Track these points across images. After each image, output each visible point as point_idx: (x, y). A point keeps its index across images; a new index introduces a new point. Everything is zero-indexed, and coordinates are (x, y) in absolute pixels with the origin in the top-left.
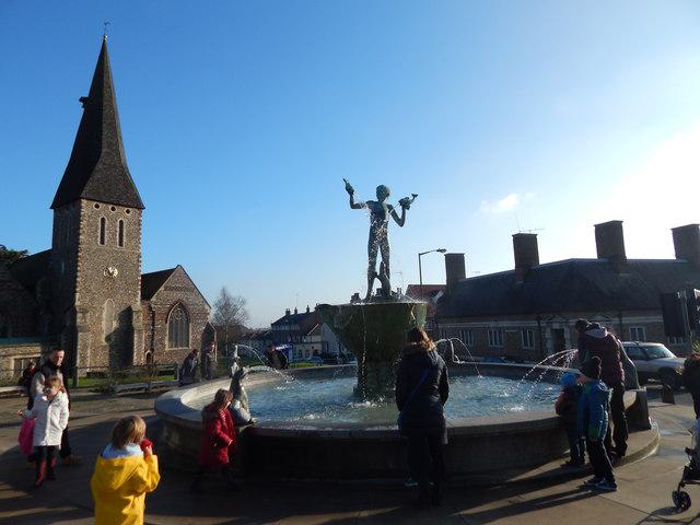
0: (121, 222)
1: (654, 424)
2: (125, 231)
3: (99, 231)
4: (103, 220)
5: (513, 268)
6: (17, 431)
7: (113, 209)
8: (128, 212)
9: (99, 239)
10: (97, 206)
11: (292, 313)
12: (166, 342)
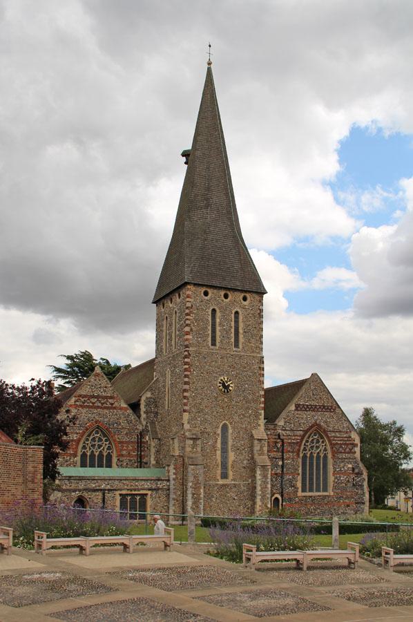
3: (210, 328)
7: (226, 296)
8: (245, 299)
12: (299, 484)
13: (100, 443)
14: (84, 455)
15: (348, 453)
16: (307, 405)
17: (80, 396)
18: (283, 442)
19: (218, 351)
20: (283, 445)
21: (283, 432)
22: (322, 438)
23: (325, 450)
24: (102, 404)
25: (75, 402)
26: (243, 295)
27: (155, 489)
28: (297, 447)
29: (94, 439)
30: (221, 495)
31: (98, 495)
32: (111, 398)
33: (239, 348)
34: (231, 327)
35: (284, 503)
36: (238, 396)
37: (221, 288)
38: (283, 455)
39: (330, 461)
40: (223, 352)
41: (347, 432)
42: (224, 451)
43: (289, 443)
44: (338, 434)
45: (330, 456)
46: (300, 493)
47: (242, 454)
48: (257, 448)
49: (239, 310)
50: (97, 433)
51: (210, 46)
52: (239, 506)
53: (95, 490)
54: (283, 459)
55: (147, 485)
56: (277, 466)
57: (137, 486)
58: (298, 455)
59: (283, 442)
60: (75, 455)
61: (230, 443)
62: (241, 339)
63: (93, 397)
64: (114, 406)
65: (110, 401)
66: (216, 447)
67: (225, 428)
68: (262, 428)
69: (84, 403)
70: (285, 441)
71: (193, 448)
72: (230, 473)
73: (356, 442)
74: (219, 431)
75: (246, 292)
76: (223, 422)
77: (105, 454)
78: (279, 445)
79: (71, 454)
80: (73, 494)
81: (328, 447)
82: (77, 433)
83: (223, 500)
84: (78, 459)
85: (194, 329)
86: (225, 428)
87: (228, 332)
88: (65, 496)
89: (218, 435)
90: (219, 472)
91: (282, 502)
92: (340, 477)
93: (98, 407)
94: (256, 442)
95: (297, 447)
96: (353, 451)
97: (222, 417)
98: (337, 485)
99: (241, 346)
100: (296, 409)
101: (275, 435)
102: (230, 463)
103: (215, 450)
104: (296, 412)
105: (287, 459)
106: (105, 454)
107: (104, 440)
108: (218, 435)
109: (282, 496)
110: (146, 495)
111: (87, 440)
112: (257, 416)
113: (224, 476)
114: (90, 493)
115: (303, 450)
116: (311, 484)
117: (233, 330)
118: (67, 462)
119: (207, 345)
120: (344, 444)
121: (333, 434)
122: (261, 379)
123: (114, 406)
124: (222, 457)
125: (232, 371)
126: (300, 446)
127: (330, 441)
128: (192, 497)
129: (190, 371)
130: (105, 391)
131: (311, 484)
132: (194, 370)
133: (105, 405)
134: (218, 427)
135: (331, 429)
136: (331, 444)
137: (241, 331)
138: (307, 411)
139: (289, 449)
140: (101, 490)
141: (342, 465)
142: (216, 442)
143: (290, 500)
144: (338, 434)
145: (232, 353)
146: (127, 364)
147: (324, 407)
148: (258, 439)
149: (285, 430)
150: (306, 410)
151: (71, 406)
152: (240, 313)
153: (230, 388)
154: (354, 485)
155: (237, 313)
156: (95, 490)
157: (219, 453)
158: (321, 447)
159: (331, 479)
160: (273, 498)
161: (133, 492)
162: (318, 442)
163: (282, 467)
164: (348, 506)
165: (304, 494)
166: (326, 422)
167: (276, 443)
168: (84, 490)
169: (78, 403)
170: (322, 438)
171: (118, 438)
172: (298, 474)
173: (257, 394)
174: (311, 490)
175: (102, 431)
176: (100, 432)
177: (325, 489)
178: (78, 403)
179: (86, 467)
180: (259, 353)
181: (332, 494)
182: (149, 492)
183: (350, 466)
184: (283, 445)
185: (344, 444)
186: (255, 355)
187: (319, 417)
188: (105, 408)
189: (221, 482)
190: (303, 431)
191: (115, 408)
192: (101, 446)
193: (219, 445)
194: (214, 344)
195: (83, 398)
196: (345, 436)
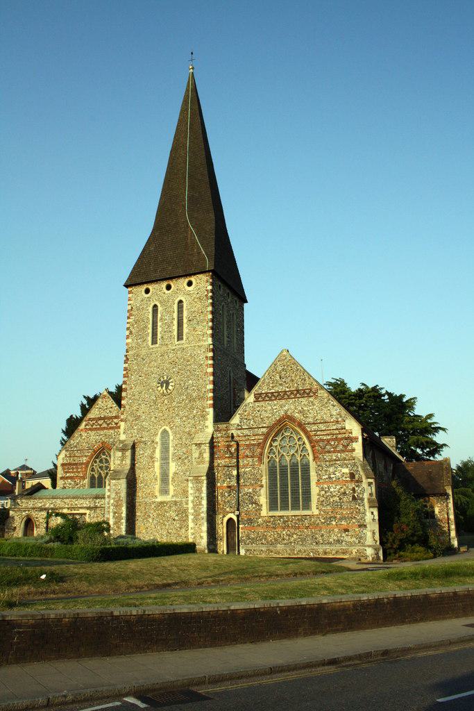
3: (150, 326)
8: (190, 284)
9: (150, 338)
12: (263, 500)
13: (101, 465)
14: (93, 478)
15: (342, 451)
16: (272, 393)
17: (90, 419)
18: (238, 445)
20: (237, 450)
21: (239, 432)
22: (297, 433)
23: (304, 449)
24: (108, 424)
25: (85, 426)
26: (187, 280)
27: (93, 508)
28: (259, 450)
30: (159, 515)
32: (116, 417)
34: (173, 319)
35: (241, 526)
36: (181, 394)
38: (238, 462)
40: (165, 348)
41: (337, 422)
42: (165, 459)
43: (247, 445)
44: (322, 427)
47: (185, 464)
51: (192, 53)
52: (181, 528)
54: (238, 467)
55: (86, 503)
56: (230, 476)
57: (76, 505)
58: (260, 460)
59: (238, 445)
60: (84, 478)
62: (185, 330)
63: (100, 419)
69: (92, 426)
70: (241, 443)
71: (122, 460)
72: (171, 488)
73: (354, 435)
74: (158, 439)
76: (163, 428)
78: (233, 450)
80: (24, 513)
81: (308, 446)
83: (161, 521)
84: (86, 481)
85: (133, 331)
87: (170, 325)
89: (157, 443)
90: (157, 487)
91: (238, 524)
93: (104, 428)
95: (259, 450)
96: (349, 448)
100: (257, 400)
101: (228, 437)
102: (171, 475)
104: (257, 404)
105: (245, 466)
108: (157, 443)
110: (85, 514)
112: (204, 417)
113: (164, 491)
116: (284, 493)
117: (175, 322)
118: (77, 485)
120: (333, 440)
121: (315, 427)
124: (162, 467)
126: (263, 448)
127: (309, 437)
128: (114, 517)
129: (128, 377)
131: (284, 493)
133: (110, 426)
135: (311, 420)
136: (310, 442)
139: (248, 453)
140: (45, 509)
141: (331, 469)
142: (154, 451)
143: (250, 521)
144: (322, 427)
146: (403, 394)
147: (298, 391)
150: (270, 400)
151: (82, 430)
152: (184, 300)
154: (354, 498)
155: (181, 302)
157: (157, 465)
159: (314, 490)
161: (73, 512)
163: (238, 476)
164: (346, 530)
165: (271, 513)
167: (229, 446)
168: (34, 508)
169: (87, 427)
170: (297, 433)
172: (262, 486)
173: (204, 390)
174: (285, 508)
177: (307, 506)
178: (87, 427)
179: (95, 487)
181: (316, 512)
182: (88, 512)
183: (346, 470)
184: (237, 450)
185: (333, 440)
186: (201, 343)
188: (111, 428)
189: (160, 499)
190: (267, 427)
193: (158, 454)
196: (334, 427)
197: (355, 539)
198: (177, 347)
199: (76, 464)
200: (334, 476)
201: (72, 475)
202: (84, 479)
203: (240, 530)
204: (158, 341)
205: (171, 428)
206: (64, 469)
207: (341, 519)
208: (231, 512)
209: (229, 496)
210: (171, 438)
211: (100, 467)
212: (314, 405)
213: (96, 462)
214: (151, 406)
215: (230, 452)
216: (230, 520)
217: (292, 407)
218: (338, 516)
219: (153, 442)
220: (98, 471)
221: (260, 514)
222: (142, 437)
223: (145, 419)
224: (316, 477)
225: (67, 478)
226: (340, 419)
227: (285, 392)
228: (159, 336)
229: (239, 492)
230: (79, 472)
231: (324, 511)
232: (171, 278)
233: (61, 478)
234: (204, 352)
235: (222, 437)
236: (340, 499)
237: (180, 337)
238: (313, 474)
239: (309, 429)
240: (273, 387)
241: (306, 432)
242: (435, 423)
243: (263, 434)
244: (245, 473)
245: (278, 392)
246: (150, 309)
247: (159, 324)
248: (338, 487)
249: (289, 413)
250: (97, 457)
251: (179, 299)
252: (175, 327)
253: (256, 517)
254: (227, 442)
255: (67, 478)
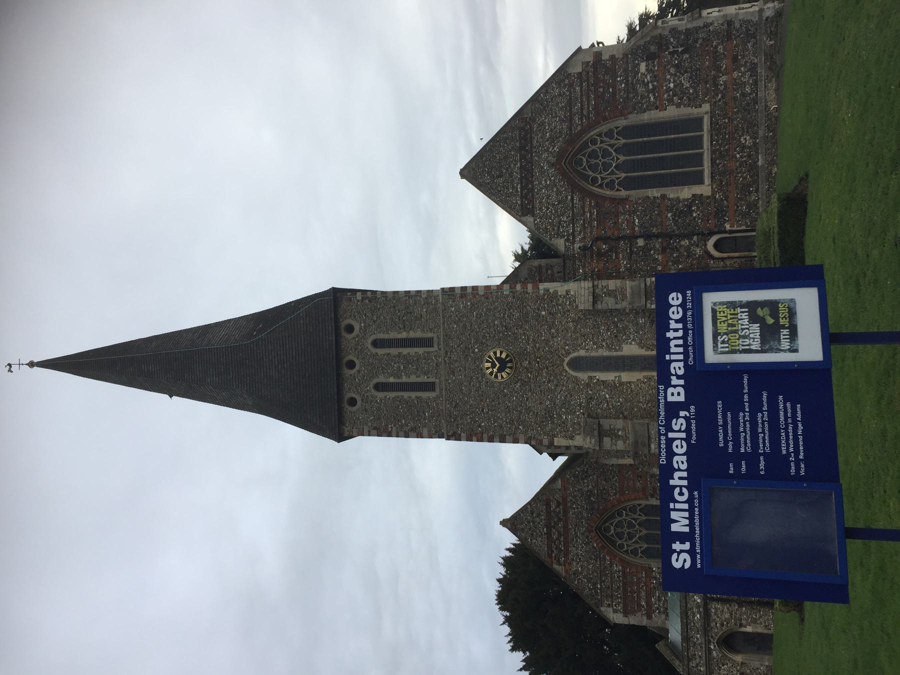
0: (375, 344)
1: (624, 618)
2: (393, 335)
3: (406, 395)
4: (379, 387)
5: (672, 530)
6: (683, 441)
7: (351, 364)
8: (350, 329)
9: (425, 395)
10: (353, 402)
11: (520, 252)
12: (685, 193)
15: (614, 76)
17: (550, 556)
19: (443, 378)
20: (605, 240)
22: (585, 146)
23: (609, 134)
24: (560, 520)
25: (560, 564)
26: (344, 334)
28: (607, 204)
29: (593, 167)
31: (716, 609)
33: (433, 338)
37: (339, 375)
39: (635, 119)
45: (622, 122)
46: (704, 189)
48: (609, 303)
49: (370, 340)
50: (579, 162)
53: (706, 615)
54: (632, 238)
56: (646, 249)
61: (604, 353)
62: (418, 334)
63: (549, 534)
64: (561, 500)
65: (553, 506)
66: (614, 381)
67: (577, 364)
68: (572, 286)
69: (561, 551)
74: (583, 376)
75: (340, 400)
76: (567, 368)
77: (644, 518)
79: (647, 576)
81: (604, 128)
82: (611, 564)
86: (577, 364)
88: (720, 668)
89: (591, 378)
91: (725, 232)
92: (669, 90)
94: (599, 306)
95: (607, 204)
96: (609, 63)
97: (557, 371)
98: (683, 97)
99: (430, 335)
101: (585, 256)
103: (621, 384)
106: (644, 518)
107: (620, 519)
108: (591, 378)
109: (712, 234)
111: (595, 180)
114: (713, 624)
115: (612, 189)
116: (676, 162)
119: (435, 399)
121: (576, 119)
122: (469, 291)
123: (561, 500)
125: (473, 352)
126: (604, 198)
127: (591, 127)
130: (539, 515)
131: (676, 162)
132: (480, 426)
133: (561, 515)
134: (577, 381)
136: (597, 123)
137: (404, 335)
138: (533, 189)
139: (610, 223)
141: (641, 89)
145: (442, 352)
147: (522, 148)
148: (594, 302)
149: (573, 234)
151: (566, 571)
152: (374, 337)
153: (503, 356)
155: (375, 344)
156: (706, 615)
157: (626, 377)
158: (604, 146)
159: (672, 112)
160: (716, 254)
162: (593, 155)
164: (735, 59)
165: (707, 181)
166: (552, 140)
167: (600, 254)
170: (585, 146)
171: (615, 494)
172: (663, 197)
173: (510, 299)
174: (698, 160)
175: (605, 522)
176: (579, 157)
177: (696, 123)
180: (436, 298)
181: (706, 107)
184: (605, 240)
187: (544, 159)
190: (573, 193)
191: (564, 499)
192: (605, 150)
194: (429, 387)
195: (553, 551)
197: (749, 45)
198: (442, 346)
199: (625, 584)
200: (650, 85)
201: (643, 594)
202: (650, 568)
203: (735, 228)
204: (431, 380)
205: (568, 353)
206: (633, 612)
207: (718, 69)
208: (706, 245)
209: (678, 250)
210: (582, 353)
211: (630, 539)
212: (543, 123)
213: (621, 546)
214: (530, 390)
215: (607, 251)
216: (716, 246)
217: (545, 155)
218: (713, 73)
219: (588, 385)
220: (636, 542)
221: (708, 197)
222: (580, 405)
223: (551, 400)
224: (652, 112)
225: (649, 604)
226: (567, 81)
227: (521, 167)
228: (424, 379)
229: (670, 236)
230: (638, 579)
231: (705, 95)
232: (338, 358)
233: (649, 617)
234: (454, 301)
235: (584, 267)
236: (686, 72)
237: (428, 343)
238: (647, 117)
239: (579, 128)
240: (513, 188)
241: (584, 131)
242: (623, 40)
243: (582, 200)
244: (641, 226)
245: (521, 179)
246: (380, 395)
247: (404, 379)
248: (668, 77)
249: (553, 160)
250: (613, 543)
251: (370, 347)
252: (412, 351)
253: (712, 203)
254: (592, 257)
255: (649, 604)
